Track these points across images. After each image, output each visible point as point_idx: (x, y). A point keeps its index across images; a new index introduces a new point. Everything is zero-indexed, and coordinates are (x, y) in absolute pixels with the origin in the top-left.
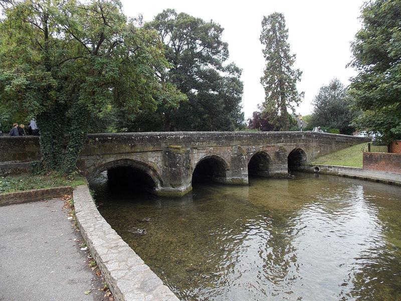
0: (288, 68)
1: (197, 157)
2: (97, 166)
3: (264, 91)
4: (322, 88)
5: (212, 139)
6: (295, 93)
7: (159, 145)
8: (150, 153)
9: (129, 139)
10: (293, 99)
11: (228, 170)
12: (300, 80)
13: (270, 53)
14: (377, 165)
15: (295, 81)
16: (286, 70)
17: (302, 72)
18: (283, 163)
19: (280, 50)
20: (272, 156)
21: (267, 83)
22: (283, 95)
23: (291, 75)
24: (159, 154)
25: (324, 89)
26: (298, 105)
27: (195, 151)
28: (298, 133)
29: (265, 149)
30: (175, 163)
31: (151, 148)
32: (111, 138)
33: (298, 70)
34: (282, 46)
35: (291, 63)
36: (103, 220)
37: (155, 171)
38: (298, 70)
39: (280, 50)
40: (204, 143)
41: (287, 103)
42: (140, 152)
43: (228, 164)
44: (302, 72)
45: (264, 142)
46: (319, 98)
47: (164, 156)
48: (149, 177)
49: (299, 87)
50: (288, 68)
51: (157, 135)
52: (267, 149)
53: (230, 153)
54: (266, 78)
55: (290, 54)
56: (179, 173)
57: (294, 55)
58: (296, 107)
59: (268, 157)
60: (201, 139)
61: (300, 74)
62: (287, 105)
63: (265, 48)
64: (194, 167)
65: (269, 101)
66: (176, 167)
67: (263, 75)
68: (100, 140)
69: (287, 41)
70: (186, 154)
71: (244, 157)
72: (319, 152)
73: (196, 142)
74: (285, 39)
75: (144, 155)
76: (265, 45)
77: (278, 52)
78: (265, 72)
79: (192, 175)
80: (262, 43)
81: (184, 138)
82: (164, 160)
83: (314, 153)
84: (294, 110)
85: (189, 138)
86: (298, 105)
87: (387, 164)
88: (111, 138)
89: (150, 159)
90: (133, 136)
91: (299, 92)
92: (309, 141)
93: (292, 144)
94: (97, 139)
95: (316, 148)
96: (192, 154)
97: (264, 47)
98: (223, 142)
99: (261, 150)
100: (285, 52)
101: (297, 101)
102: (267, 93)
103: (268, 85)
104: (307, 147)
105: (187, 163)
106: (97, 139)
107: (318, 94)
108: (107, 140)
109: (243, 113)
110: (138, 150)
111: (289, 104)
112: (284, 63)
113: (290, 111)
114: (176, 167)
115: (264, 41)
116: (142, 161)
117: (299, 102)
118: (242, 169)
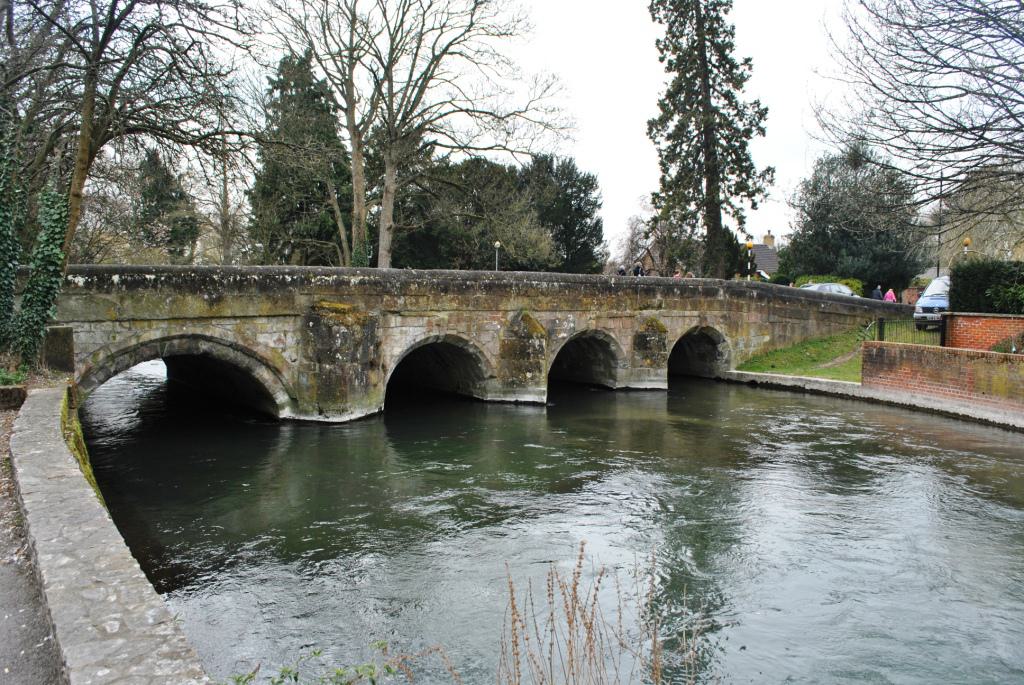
0: (728, 96)
1: (400, 338)
2: (114, 350)
3: (655, 160)
4: (820, 162)
5: (446, 290)
6: (748, 170)
7: (290, 299)
8: (264, 320)
9: (204, 282)
10: (741, 187)
11: (492, 377)
12: (762, 131)
13: (676, 48)
14: (892, 376)
15: (747, 133)
16: (723, 101)
17: (766, 109)
18: (655, 364)
19: (708, 44)
20: (624, 344)
21: (669, 137)
22: (714, 173)
23: (737, 118)
24: (289, 325)
25: (828, 165)
26: (754, 206)
27: (395, 320)
28: (705, 283)
29: (602, 324)
30: (330, 350)
31: (265, 307)
32: (153, 277)
33: (757, 103)
34: (713, 32)
35: (739, 82)
36: (115, 527)
37: (276, 372)
38: (757, 103)
39: (708, 44)
40: (421, 300)
41: (722, 196)
42: (235, 317)
43: (494, 362)
44: (766, 109)
45: (601, 305)
46: (813, 187)
47: (304, 329)
48: (206, 355)
49: (758, 150)
50: (728, 96)
51: (284, 274)
52: (611, 324)
53: (497, 331)
54: (664, 120)
55: (737, 56)
56: (343, 380)
57: (747, 61)
58: (748, 212)
59: (613, 348)
60: (413, 287)
61: (763, 114)
62: (722, 202)
63: (662, 37)
64: (392, 366)
65: (673, 193)
66: (333, 361)
67: (657, 113)
68: (123, 282)
69: (728, 20)
70: (363, 325)
71: (537, 343)
72: (767, 338)
73: (399, 297)
74: (722, 14)
75: (247, 326)
76: (665, 27)
77: (702, 48)
78: (662, 105)
79: (382, 388)
80: (654, 19)
81: (362, 283)
82: (305, 341)
83: (754, 341)
84: (741, 221)
85: (376, 283)
86: (754, 206)
87: (914, 373)
88: (153, 277)
89: (261, 339)
90: (217, 274)
91: (759, 168)
92: (739, 308)
93: (687, 313)
94: (116, 278)
95: (760, 328)
96: (387, 327)
97: (661, 31)
98: (477, 300)
99: (593, 324)
100: (721, 49)
101: (751, 195)
102: (665, 170)
103: (669, 143)
104: (734, 326)
105: (365, 352)
106: (116, 278)
107: (809, 176)
108: (144, 283)
109: (599, 222)
110: (228, 313)
111: (727, 200)
112: (718, 80)
113: (728, 221)
114: (333, 361)
115: (662, 13)
116: (241, 342)
117: (757, 198)
118: (529, 375)
